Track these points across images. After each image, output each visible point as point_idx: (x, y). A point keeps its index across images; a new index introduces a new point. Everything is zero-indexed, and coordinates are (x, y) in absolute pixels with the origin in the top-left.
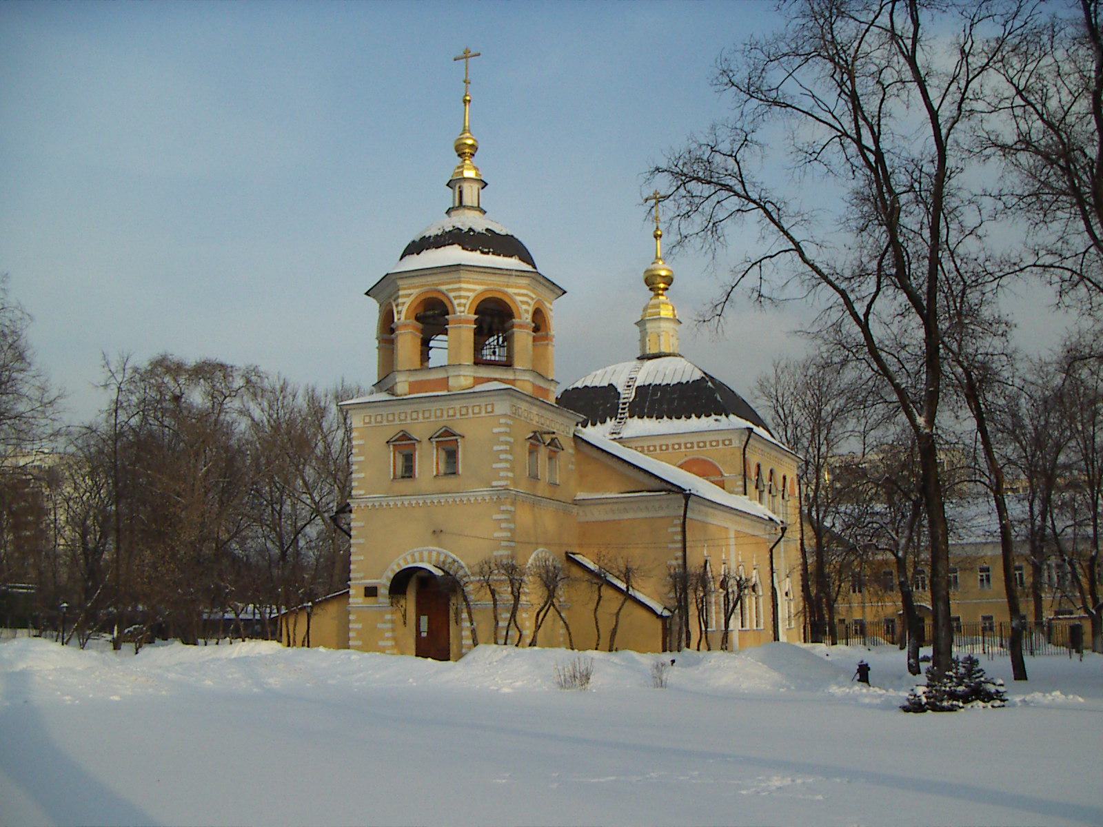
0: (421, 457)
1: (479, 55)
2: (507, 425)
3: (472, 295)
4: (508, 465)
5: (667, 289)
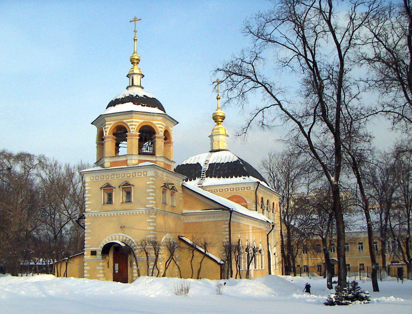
3: (137, 124)
4: (153, 198)
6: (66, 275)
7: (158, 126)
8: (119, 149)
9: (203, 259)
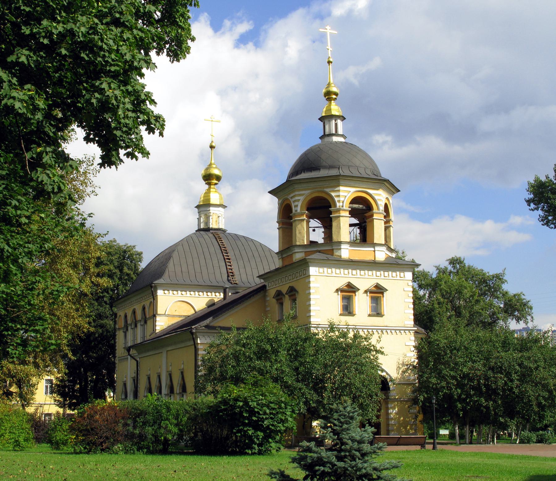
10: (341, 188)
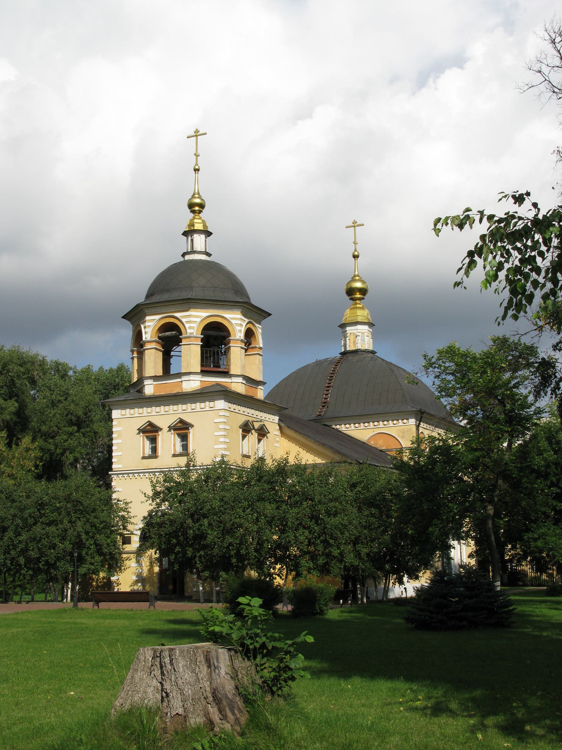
0: (163, 440)
1: (206, 134)
2: (225, 443)
3: (199, 320)
4: (225, 446)
5: (363, 299)
6: (19, 602)
7: (233, 322)
8: (171, 359)
9: (355, 237)
10: (148, 318)
